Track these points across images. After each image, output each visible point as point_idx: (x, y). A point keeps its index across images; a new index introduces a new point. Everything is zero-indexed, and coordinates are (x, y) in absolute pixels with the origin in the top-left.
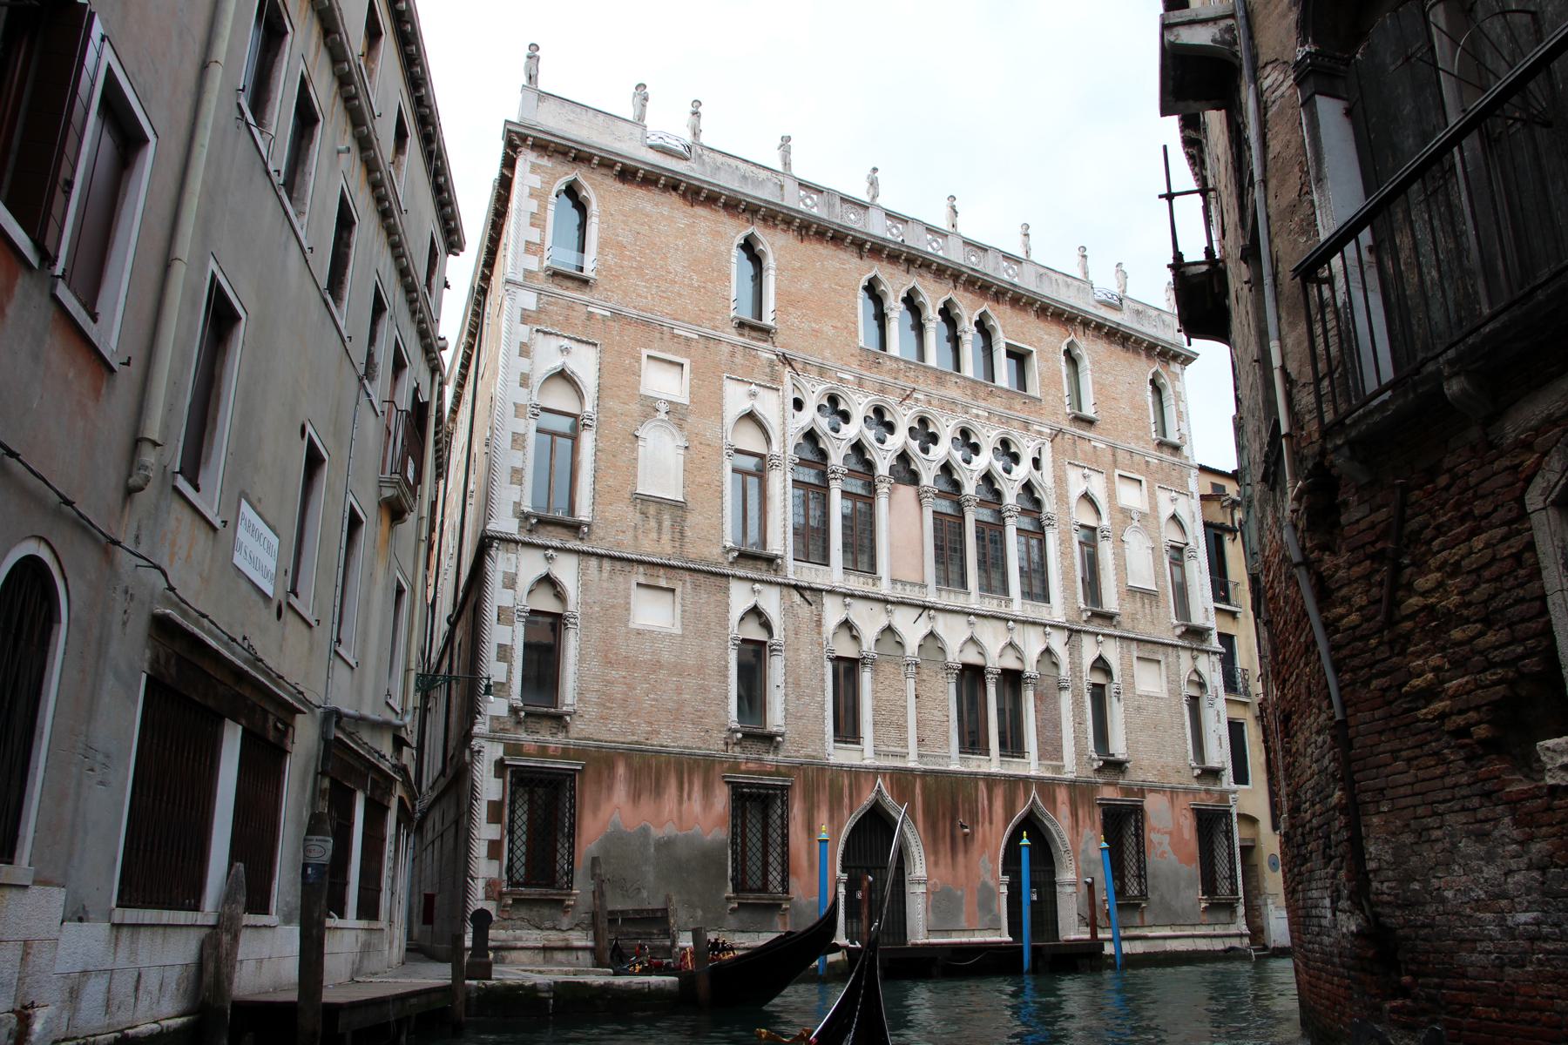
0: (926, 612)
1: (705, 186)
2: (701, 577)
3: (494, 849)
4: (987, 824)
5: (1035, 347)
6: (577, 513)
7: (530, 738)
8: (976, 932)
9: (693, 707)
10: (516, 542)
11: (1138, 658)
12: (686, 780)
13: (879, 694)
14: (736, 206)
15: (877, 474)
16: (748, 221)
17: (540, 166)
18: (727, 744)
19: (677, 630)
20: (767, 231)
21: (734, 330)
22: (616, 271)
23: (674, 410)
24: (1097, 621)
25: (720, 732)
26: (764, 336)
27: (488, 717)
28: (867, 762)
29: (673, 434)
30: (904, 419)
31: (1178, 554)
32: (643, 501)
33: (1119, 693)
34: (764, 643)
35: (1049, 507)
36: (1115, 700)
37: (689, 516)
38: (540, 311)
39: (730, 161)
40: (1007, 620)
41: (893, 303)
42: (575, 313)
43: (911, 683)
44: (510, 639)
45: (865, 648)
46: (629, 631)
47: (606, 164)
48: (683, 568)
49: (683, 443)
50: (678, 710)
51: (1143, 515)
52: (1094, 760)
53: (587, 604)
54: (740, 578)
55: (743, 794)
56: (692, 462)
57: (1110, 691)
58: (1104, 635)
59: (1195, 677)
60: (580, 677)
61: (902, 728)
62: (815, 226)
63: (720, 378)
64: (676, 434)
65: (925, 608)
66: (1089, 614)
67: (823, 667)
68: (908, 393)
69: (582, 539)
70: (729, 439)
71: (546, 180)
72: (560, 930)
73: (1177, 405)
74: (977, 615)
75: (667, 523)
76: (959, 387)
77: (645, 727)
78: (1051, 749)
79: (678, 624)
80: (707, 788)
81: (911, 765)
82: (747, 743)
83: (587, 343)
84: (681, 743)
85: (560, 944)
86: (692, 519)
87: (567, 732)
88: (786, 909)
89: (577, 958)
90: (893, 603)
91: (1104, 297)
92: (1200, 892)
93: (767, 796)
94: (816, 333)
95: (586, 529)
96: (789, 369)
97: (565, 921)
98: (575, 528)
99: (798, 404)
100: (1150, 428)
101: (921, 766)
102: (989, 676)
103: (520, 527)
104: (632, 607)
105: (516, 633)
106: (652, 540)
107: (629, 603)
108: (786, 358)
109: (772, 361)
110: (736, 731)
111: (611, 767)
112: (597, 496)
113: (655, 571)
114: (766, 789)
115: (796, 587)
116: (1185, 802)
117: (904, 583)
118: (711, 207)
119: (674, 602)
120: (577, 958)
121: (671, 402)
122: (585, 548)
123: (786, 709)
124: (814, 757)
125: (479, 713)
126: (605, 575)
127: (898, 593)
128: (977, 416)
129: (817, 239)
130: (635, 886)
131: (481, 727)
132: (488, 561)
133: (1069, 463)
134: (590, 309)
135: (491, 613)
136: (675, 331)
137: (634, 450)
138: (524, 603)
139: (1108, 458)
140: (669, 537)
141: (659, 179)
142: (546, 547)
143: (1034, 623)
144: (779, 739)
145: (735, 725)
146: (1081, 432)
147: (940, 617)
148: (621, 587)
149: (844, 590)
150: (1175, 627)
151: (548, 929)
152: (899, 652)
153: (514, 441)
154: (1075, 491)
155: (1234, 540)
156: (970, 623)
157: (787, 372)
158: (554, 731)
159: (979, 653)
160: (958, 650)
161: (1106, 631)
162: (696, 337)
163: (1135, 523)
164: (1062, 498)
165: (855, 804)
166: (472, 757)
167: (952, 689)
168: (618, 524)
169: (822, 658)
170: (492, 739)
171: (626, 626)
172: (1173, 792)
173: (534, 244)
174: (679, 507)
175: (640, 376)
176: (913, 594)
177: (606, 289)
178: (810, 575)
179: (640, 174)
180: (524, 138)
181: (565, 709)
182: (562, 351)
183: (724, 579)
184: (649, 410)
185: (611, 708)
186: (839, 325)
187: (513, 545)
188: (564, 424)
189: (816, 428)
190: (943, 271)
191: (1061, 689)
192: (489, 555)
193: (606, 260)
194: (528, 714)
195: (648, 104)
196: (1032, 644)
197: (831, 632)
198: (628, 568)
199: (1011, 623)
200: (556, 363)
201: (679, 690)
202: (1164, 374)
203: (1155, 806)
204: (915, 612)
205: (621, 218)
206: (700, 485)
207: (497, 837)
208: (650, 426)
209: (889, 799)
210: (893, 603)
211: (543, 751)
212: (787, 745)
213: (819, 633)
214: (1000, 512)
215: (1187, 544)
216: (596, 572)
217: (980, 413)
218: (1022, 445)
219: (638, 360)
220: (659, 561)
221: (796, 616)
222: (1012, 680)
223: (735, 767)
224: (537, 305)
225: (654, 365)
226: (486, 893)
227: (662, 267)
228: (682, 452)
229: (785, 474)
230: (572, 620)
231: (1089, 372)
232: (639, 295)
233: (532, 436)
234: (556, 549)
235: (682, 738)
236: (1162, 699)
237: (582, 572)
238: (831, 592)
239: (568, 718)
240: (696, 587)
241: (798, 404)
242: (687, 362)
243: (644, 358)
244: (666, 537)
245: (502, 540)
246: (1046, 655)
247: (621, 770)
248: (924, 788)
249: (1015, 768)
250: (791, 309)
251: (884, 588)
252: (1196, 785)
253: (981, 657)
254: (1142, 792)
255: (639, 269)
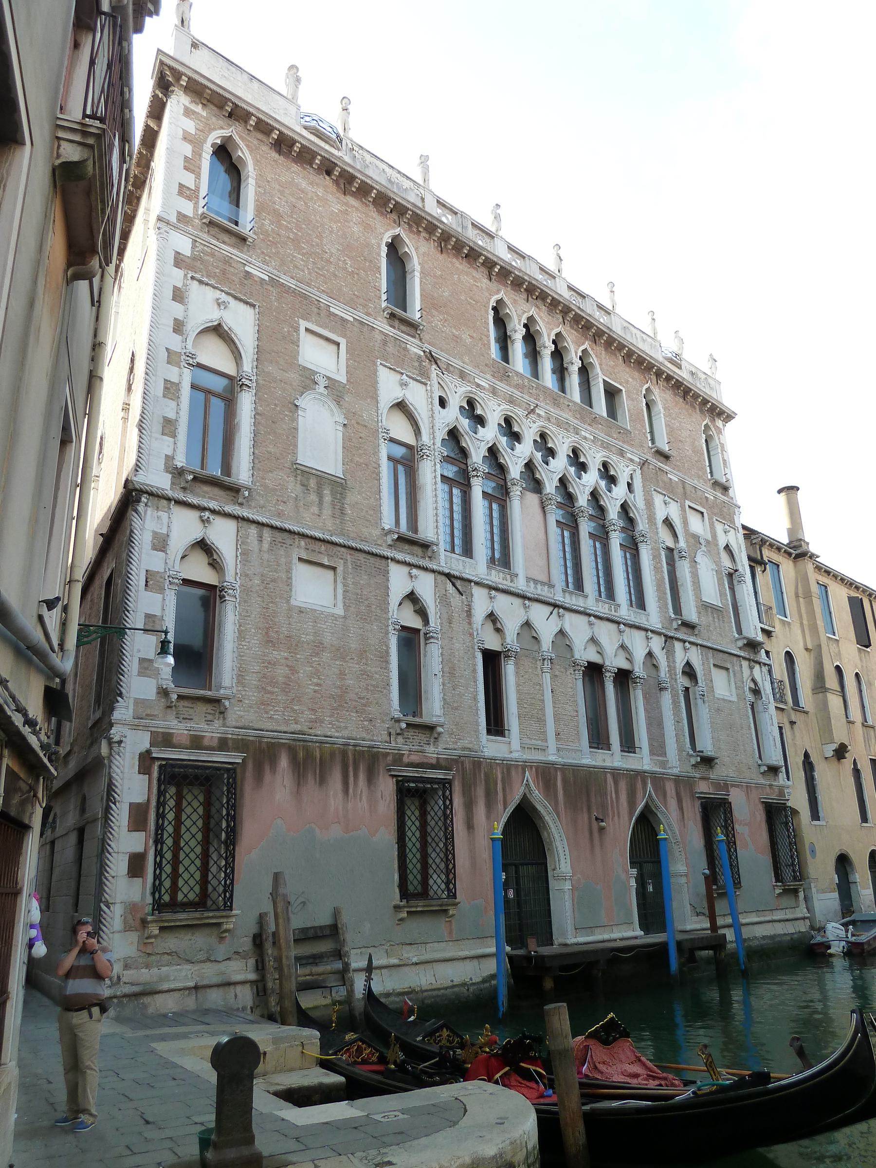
0: (556, 610)
1: (359, 175)
2: (361, 556)
3: (136, 865)
4: (616, 817)
5: (624, 387)
6: (234, 470)
7: (182, 726)
8: (614, 928)
9: (357, 694)
10: (169, 499)
11: (714, 665)
12: (351, 774)
13: (521, 687)
14: (385, 205)
15: (509, 478)
16: (395, 222)
17: (194, 112)
18: (390, 734)
19: (340, 611)
20: (412, 236)
21: (385, 321)
22: (273, 238)
23: (332, 385)
24: (684, 629)
25: (383, 722)
26: (412, 331)
27: (132, 701)
28: (515, 755)
29: (332, 410)
30: (530, 434)
31: (732, 576)
32: (304, 474)
33: (703, 695)
34: (417, 631)
35: (642, 525)
36: (700, 701)
37: (349, 494)
38: (194, 258)
39: (378, 162)
40: (618, 623)
41: (517, 325)
42: (232, 270)
43: (547, 677)
44: (159, 605)
45: (509, 640)
46: (290, 609)
47: (264, 127)
48: (344, 546)
49: (341, 419)
50: (341, 696)
51: (708, 542)
52: (691, 756)
53: (247, 575)
54: (398, 562)
55: (409, 790)
56: (350, 440)
57: (695, 694)
58: (690, 643)
59: (687, 670)
60: (240, 656)
61: (542, 721)
62: (454, 240)
63: (375, 364)
64: (335, 410)
65: (555, 606)
66: (680, 622)
67: (475, 657)
68: (532, 408)
69: (241, 504)
70: (384, 424)
71: (201, 128)
72: (215, 961)
73: (722, 454)
74: (597, 617)
75: (328, 498)
76: (570, 410)
77: (308, 715)
78: (658, 748)
79: (340, 605)
80: (371, 779)
81: (552, 758)
82: (410, 733)
83: (246, 303)
84: (345, 733)
85: (215, 980)
86: (351, 498)
87: (224, 719)
88: (453, 915)
89: (236, 996)
90: (529, 599)
91: (670, 355)
92: (774, 880)
93: (425, 791)
94: (456, 339)
95: (246, 494)
96: (434, 366)
97: (222, 950)
98: (233, 490)
99: (443, 403)
100: (706, 470)
101: (560, 760)
102: (608, 674)
103: (173, 483)
104: (294, 583)
105: (167, 602)
106: (313, 514)
107: (290, 578)
108: (432, 356)
109: (420, 357)
110: (398, 721)
111: (273, 762)
112: (256, 461)
113: (317, 546)
114: (431, 783)
115: (448, 576)
116: (755, 795)
117: (536, 582)
118: (362, 201)
119: (335, 581)
120: (236, 996)
121: (328, 378)
122: (245, 514)
123: (444, 699)
124: (470, 749)
125: (120, 695)
126: (266, 545)
127: (531, 590)
128: (585, 438)
129: (454, 254)
130: (301, 899)
131: (123, 712)
132: (131, 513)
133: (655, 490)
134: (247, 268)
135: (137, 579)
136: (332, 309)
137: (294, 419)
138: (177, 568)
139: (680, 490)
140: (330, 512)
141: (314, 158)
142: (204, 509)
143: (639, 628)
144: (440, 729)
145: (397, 714)
146: (661, 465)
147: (568, 616)
148: (283, 560)
149: (490, 583)
150: (737, 640)
151: (202, 962)
152: (536, 648)
153: (166, 388)
154: (660, 516)
155: (763, 572)
156: (591, 624)
157: (434, 370)
158: (210, 717)
159: (598, 652)
160: (583, 648)
161: (692, 639)
162: (351, 319)
163: (703, 548)
164: (651, 519)
165: (508, 798)
166: (111, 749)
167: (580, 683)
168: (278, 493)
169: (473, 648)
170: (135, 727)
171: (288, 601)
172: (748, 788)
173: (188, 188)
174: (339, 487)
175: (298, 346)
176: (543, 592)
177: (263, 253)
178: (457, 565)
179: (296, 148)
180: (178, 75)
181: (222, 691)
182: (219, 305)
183: (383, 561)
184: (308, 382)
185: (272, 693)
186: (475, 335)
187: (164, 502)
188: (219, 384)
189: (459, 427)
190: (555, 305)
191: (661, 689)
192: (136, 511)
193: (263, 224)
194: (180, 697)
195: (300, 87)
196: (639, 645)
197: (480, 623)
198: (289, 542)
199: (622, 626)
200: (213, 315)
201: (342, 674)
202: (712, 426)
203: (736, 798)
204: (547, 609)
205: (277, 187)
206: (358, 464)
207: (140, 849)
208: (309, 397)
209: (538, 798)
210: (529, 599)
211: (196, 743)
212: (445, 737)
213: (470, 623)
214: (604, 526)
215: (736, 571)
216: (256, 542)
217: (588, 436)
218: (619, 469)
219: (297, 330)
220: (321, 536)
221: (449, 605)
222: (624, 677)
223: (398, 759)
224: (192, 252)
225: (310, 338)
226: (125, 922)
227: (317, 245)
228: (341, 428)
229: (435, 464)
230: (230, 591)
231: (662, 415)
232: (296, 267)
233: (186, 391)
234: (213, 512)
235: (346, 728)
236: (733, 702)
237: (241, 541)
238: (477, 583)
239: (227, 703)
240: (357, 567)
241: (443, 403)
242: (343, 342)
243: (302, 330)
244: (327, 512)
245: (151, 494)
246: (526, 627)
247: (284, 762)
248: (565, 780)
249: (631, 763)
250: (434, 312)
251: (521, 585)
252: (762, 781)
253: (599, 655)
254: (726, 787)
255: (296, 241)
